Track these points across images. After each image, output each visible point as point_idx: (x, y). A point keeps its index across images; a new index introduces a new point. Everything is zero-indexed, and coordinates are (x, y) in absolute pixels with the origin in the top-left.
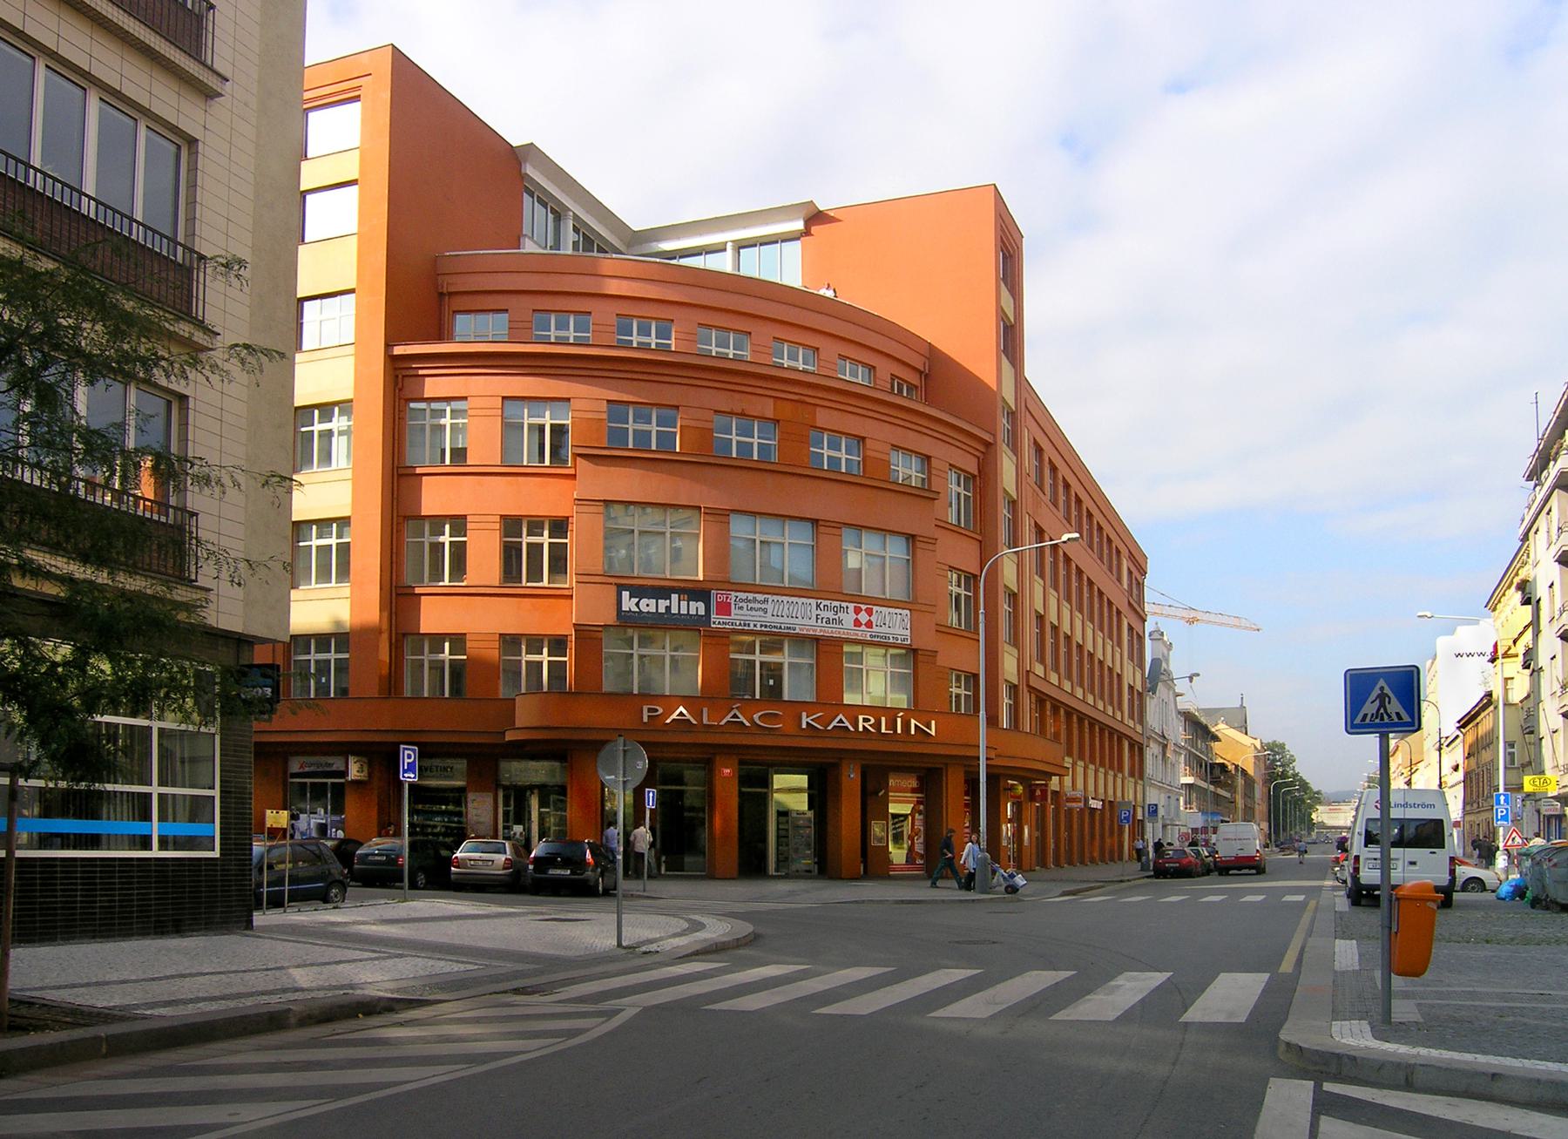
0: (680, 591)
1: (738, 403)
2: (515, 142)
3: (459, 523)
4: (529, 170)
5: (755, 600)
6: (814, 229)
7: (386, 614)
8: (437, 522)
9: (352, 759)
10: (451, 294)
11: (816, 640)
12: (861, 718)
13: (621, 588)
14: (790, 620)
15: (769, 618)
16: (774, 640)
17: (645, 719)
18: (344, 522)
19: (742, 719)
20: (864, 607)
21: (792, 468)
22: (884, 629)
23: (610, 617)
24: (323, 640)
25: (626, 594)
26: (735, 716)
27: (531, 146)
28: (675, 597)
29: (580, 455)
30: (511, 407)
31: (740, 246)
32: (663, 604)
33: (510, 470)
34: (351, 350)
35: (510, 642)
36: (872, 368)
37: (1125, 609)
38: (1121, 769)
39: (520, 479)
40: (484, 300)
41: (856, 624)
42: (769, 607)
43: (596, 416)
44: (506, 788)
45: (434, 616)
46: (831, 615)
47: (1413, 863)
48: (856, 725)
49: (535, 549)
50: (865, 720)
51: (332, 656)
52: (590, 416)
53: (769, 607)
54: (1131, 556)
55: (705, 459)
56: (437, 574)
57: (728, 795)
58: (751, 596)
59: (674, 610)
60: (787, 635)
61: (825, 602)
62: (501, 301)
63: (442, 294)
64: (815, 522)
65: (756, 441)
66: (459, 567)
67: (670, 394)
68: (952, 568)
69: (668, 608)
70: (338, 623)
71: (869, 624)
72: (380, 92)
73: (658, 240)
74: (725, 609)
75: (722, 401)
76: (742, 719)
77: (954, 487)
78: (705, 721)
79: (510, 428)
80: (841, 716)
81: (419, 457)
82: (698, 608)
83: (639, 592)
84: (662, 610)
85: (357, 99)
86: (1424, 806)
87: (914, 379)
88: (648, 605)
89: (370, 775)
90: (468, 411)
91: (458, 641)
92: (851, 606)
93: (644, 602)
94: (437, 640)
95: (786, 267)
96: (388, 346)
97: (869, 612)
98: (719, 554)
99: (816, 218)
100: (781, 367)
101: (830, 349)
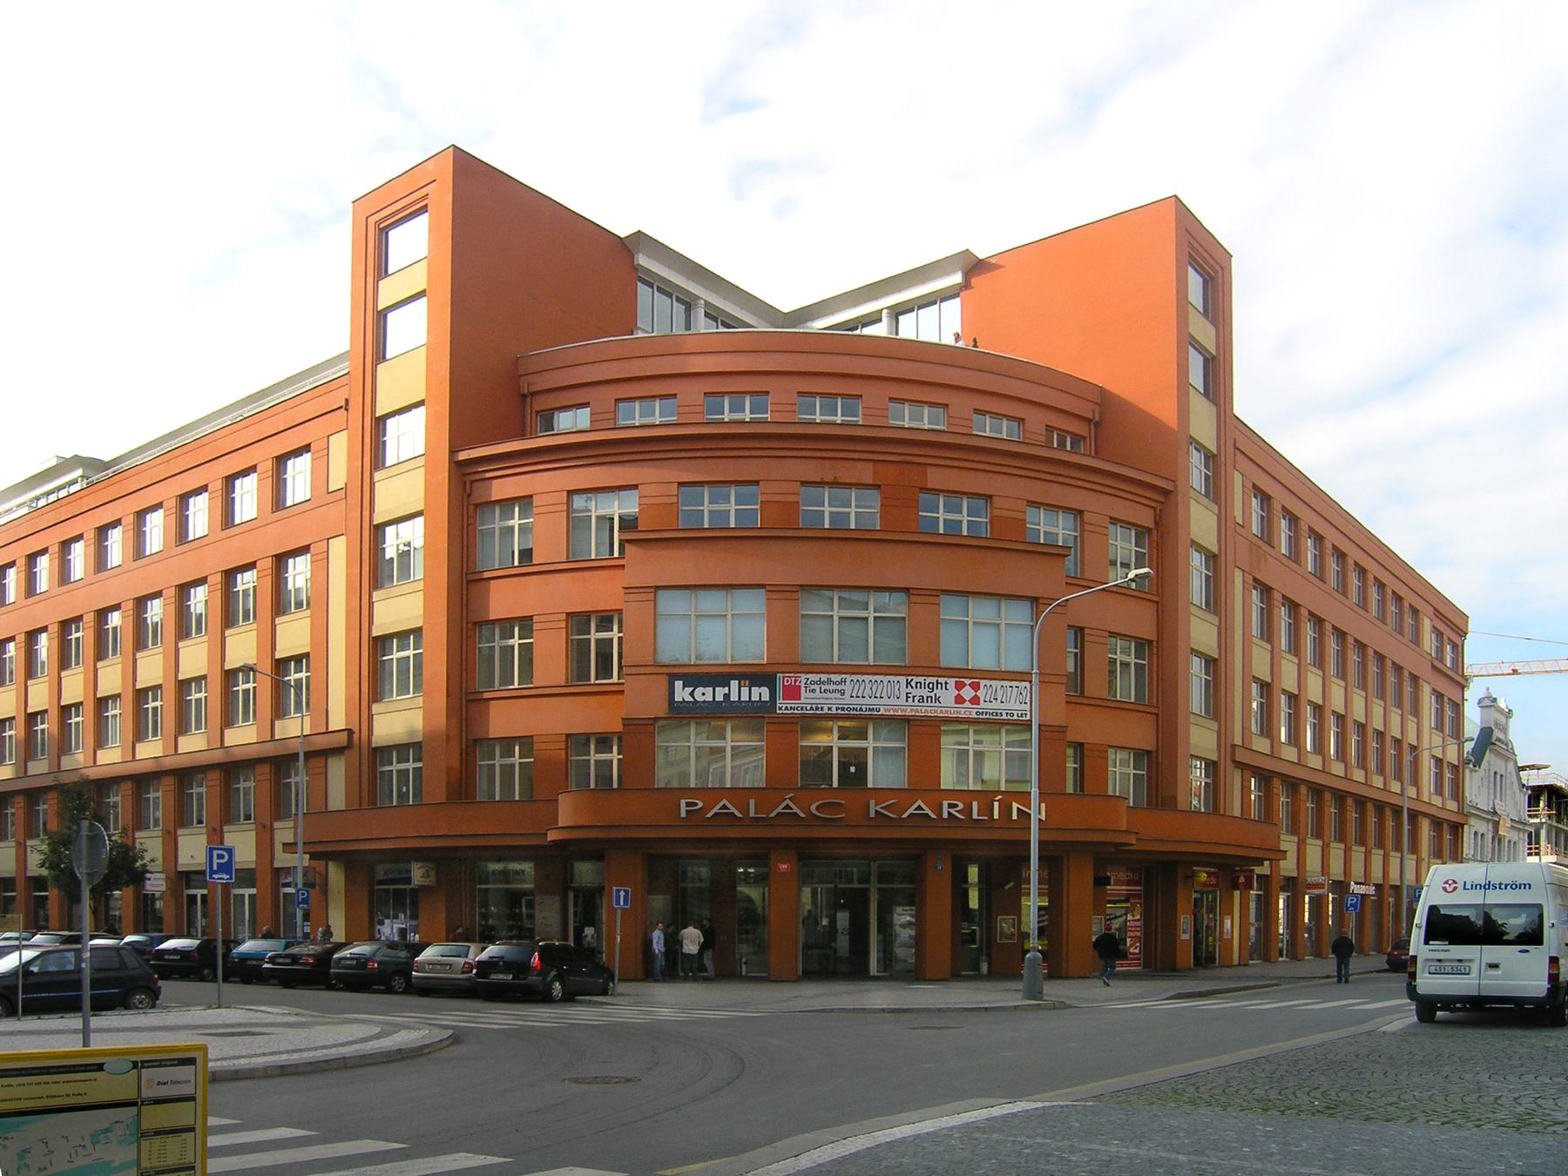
0: (740, 677)
1: (827, 471)
2: (622, 235)
3: (526, 624)
4: (642, 260)
5: (830, 681)
6: (974, 281)
7: (455, 721)
8: (506, 625)
9: (331, 864)
10: (533, 394)
11: (906, 720)
12: (945, 803)
13: (673, 677)
14: (873, 701)
15: (847, 700)
16: (858, 723)
17: (683, 814)
18: (417, 631)
19: (796, 810)
20: (967, 681)
21: (900, 532)
22: (995, 705)
23: (660, 709)
24: (403, 749)
25: (679, 684)
26: (787, 807)
27: (639, 235)
28: (734, 684)
29: (630, 541)
30: (579, 502)
31: (897, 312)
32: (720, 692)
33: (576, 566)
34: (422, 461)
35: (578, 741)
36: (1021, 421)
37: (1424, 671)
38: (1414, 848)
39: (587, 574)
40: (573, 394)
41: (971, 701)
42: (847, 688)
43: (667, 500)
44: (576, 890)
45: (502, 720)
46: (925, 692)
47: (1494, 966)
48: (940, 813)
49: (604, 646)
50: (950, 806)
51: (411, 765)
52: (657, 501)
53: (847, 688)
54: (1438, 614)
55: (783, 530)
56: (507, 678)
57: (845, 887)
58: (824, 677)
59: (734, 698)
60: (870, 718)
61: (916, 679)
62: (582, 395)
63: (524, 396)
64: (906, 590)
65: (853, 510)
66: (527, 673)
67: (747, 469)
68: (1113, 634)
69: (727, 696)
70: (412, 732)
71: (975, 700)
72: (442, 197)
73: (813, 319)
74: (793, 692)
75: (810, 470)
76: (796, 810)
77: (1122, 544)
78: (752, 814)
79: (576, 524)
80: (919, 802)
81: (492, 557)
82: (761, 693)
83: (694, 679)
84: (720, 698)
85: (424, 210)
86: (1515, 886)
87: (1080, 428)
88: (704, 694)
89: (438, 880)
90: (536, 512)
91: (526, 742)
92: (952, 682)
93: (699, 690)
94: (507, 743)
95: (939, 326)
96: (453, 452)
97: (976, 687)
98: (783, 632)
99: (974, 267)
100: (813, 423)
101: (962, 405)
